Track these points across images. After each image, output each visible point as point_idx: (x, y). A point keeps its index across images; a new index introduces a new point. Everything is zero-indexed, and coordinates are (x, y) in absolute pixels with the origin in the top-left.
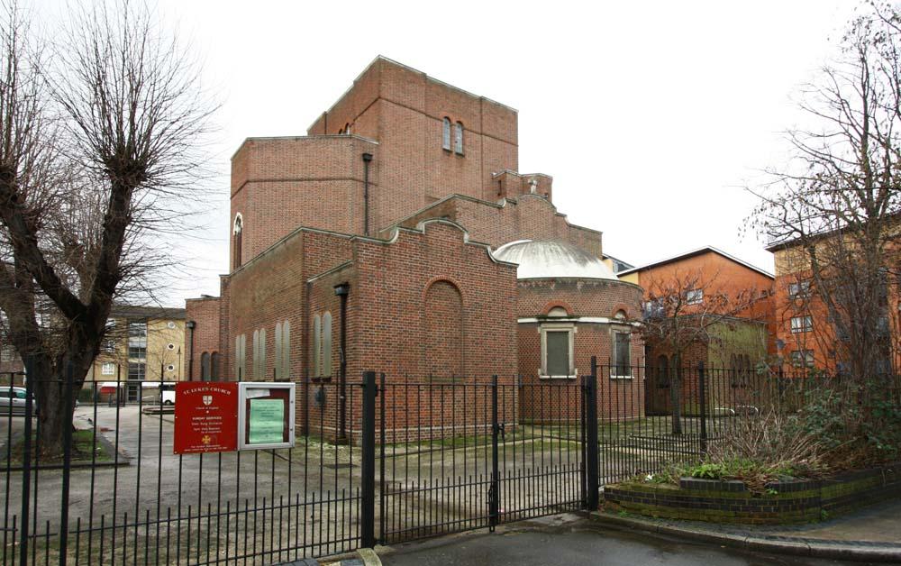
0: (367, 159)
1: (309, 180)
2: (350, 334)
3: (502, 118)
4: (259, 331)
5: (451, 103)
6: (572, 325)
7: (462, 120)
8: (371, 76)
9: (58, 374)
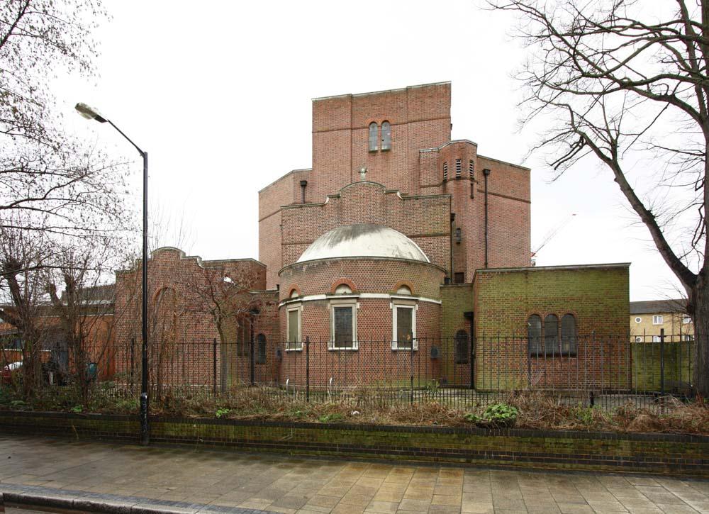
6: (355, 301)
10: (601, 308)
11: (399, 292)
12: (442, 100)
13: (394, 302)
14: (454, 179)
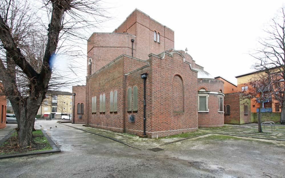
0: (132, 41)
1: (114, 47)
2: (148, 93)
3: (170, 33)
4: (102, 95)
5: (156, 27)
6: (207, 94)
7: (159, 32)
8: (133, 15)
9: (27, 109)
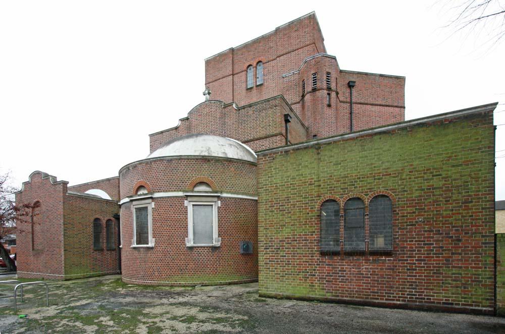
10: (436, 182)
11: (197, 189)
12: (306, 30)
13: (189, 199)
14: (310, 92)
